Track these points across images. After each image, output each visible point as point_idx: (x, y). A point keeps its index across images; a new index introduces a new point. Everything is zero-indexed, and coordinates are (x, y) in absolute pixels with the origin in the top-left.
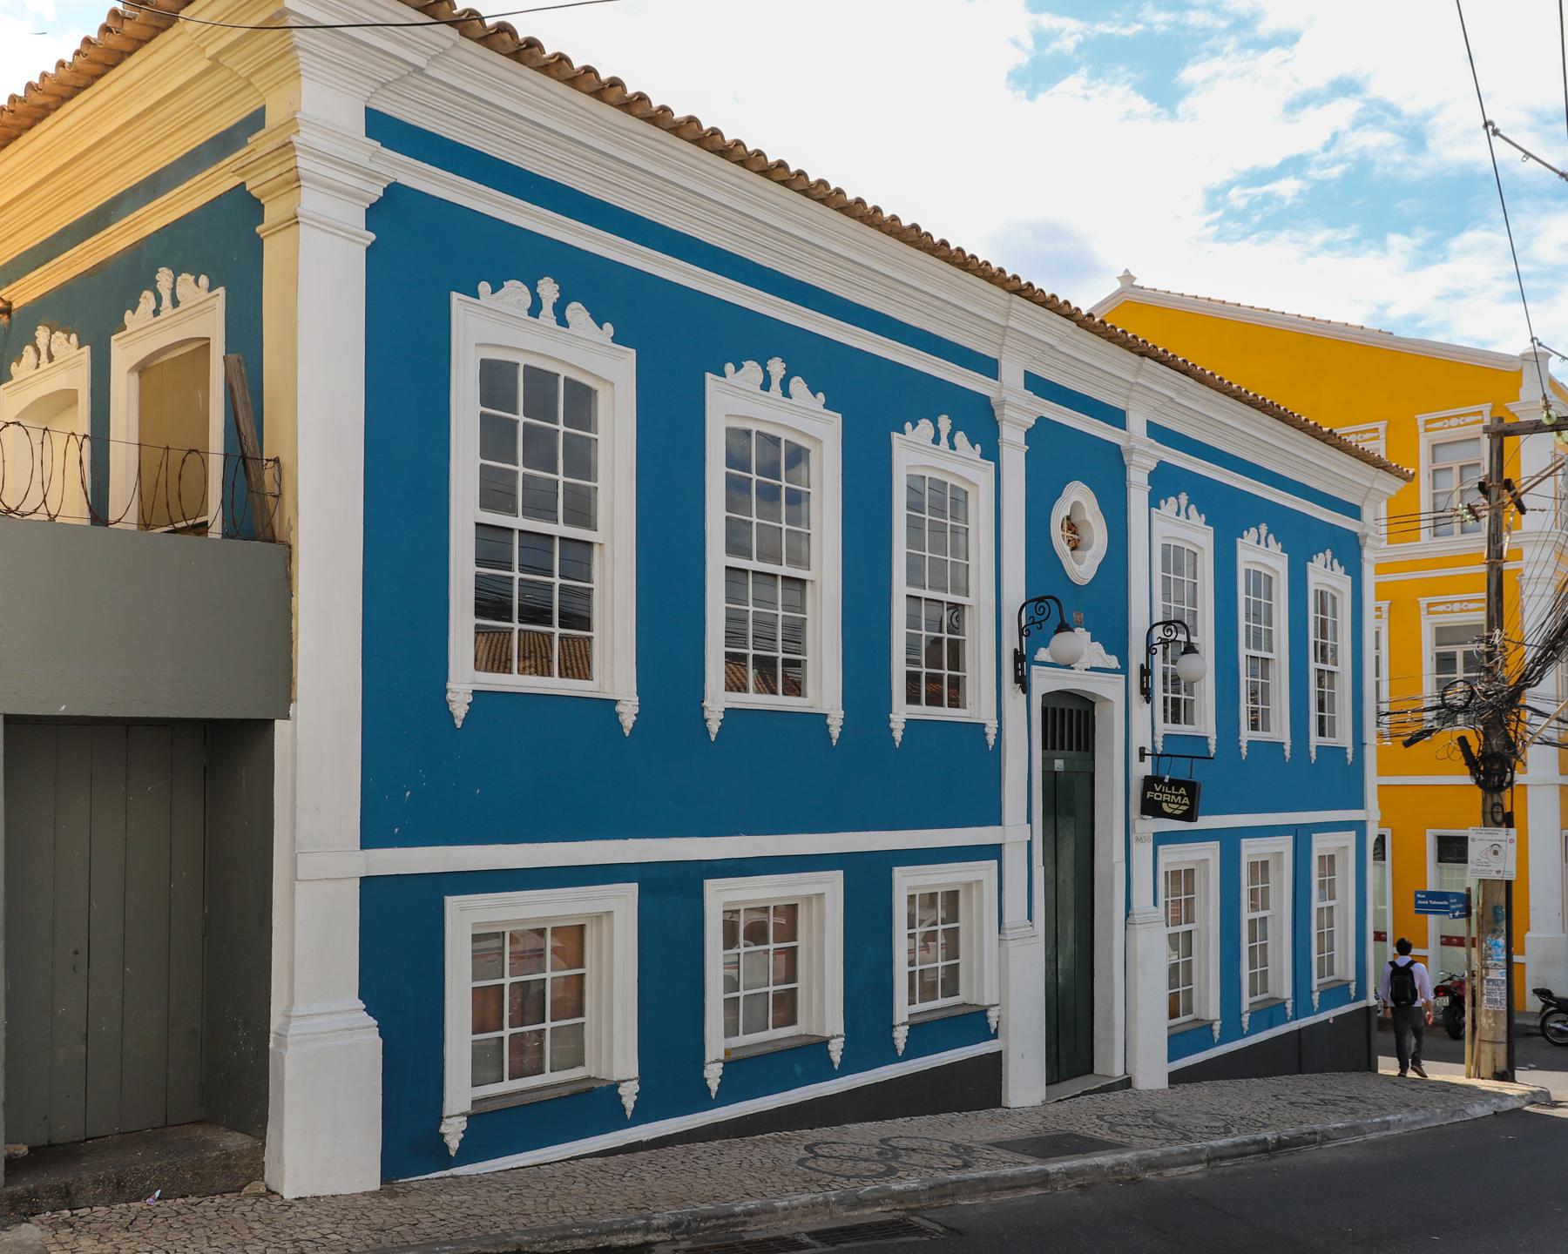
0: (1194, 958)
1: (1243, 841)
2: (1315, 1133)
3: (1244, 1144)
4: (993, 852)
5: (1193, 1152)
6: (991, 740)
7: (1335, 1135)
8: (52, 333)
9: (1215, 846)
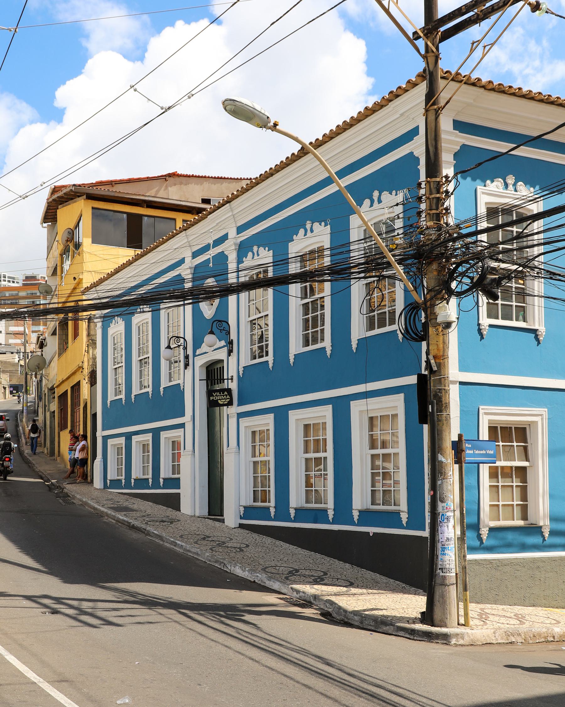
0: (171, 464)
1: (351, 402)
2: (145, 530)
3: (125, 521)
4: (182, 426)
5: (115, 516)
6: (182, 388)
7: (152, 534)
8: (313, 223)
9: (272, 416)
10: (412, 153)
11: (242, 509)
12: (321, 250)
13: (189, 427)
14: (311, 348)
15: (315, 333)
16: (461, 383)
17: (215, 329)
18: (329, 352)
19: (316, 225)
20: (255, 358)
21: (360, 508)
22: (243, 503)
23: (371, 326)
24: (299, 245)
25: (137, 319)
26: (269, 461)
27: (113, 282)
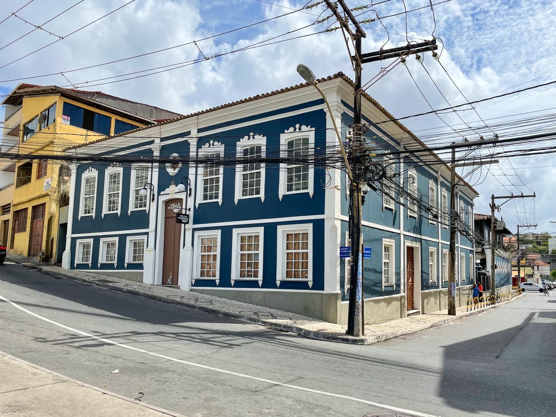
4: (147, 234)
9: (219, 231)
10: (322, 110)
11: (194, 281)
12: (259, 148)
13: (152, 236)
14: (111, 212)
15: (114, 207)
16: (342, 220)
17: (183, 182)
18: (94, 218)
19: (93, 169)
20: (137, 207)
21: (234, 279)
22: (195, 277)
23: (110, 210)
24: (244, 143)
25: (109, 171)
26: (307, 253)
27: (182, 123)
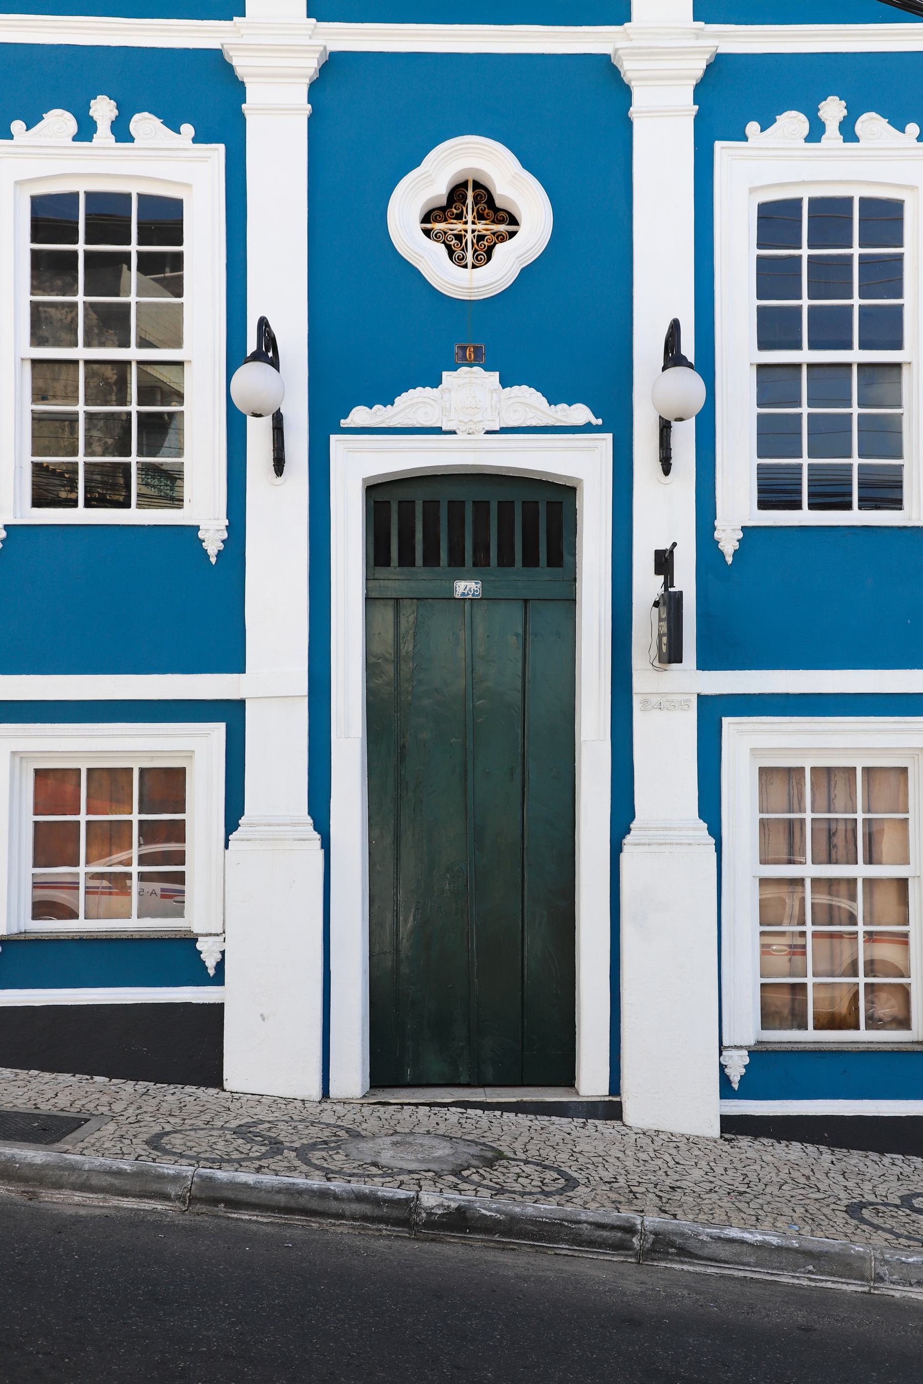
4: (232, 713)
